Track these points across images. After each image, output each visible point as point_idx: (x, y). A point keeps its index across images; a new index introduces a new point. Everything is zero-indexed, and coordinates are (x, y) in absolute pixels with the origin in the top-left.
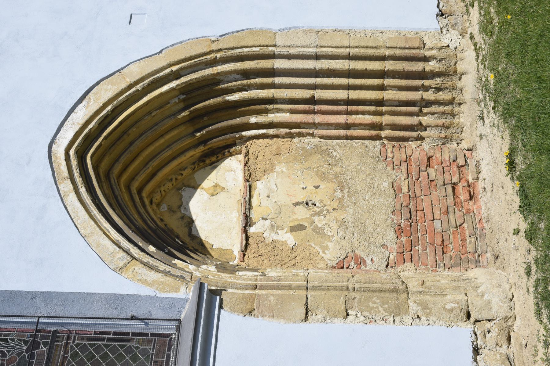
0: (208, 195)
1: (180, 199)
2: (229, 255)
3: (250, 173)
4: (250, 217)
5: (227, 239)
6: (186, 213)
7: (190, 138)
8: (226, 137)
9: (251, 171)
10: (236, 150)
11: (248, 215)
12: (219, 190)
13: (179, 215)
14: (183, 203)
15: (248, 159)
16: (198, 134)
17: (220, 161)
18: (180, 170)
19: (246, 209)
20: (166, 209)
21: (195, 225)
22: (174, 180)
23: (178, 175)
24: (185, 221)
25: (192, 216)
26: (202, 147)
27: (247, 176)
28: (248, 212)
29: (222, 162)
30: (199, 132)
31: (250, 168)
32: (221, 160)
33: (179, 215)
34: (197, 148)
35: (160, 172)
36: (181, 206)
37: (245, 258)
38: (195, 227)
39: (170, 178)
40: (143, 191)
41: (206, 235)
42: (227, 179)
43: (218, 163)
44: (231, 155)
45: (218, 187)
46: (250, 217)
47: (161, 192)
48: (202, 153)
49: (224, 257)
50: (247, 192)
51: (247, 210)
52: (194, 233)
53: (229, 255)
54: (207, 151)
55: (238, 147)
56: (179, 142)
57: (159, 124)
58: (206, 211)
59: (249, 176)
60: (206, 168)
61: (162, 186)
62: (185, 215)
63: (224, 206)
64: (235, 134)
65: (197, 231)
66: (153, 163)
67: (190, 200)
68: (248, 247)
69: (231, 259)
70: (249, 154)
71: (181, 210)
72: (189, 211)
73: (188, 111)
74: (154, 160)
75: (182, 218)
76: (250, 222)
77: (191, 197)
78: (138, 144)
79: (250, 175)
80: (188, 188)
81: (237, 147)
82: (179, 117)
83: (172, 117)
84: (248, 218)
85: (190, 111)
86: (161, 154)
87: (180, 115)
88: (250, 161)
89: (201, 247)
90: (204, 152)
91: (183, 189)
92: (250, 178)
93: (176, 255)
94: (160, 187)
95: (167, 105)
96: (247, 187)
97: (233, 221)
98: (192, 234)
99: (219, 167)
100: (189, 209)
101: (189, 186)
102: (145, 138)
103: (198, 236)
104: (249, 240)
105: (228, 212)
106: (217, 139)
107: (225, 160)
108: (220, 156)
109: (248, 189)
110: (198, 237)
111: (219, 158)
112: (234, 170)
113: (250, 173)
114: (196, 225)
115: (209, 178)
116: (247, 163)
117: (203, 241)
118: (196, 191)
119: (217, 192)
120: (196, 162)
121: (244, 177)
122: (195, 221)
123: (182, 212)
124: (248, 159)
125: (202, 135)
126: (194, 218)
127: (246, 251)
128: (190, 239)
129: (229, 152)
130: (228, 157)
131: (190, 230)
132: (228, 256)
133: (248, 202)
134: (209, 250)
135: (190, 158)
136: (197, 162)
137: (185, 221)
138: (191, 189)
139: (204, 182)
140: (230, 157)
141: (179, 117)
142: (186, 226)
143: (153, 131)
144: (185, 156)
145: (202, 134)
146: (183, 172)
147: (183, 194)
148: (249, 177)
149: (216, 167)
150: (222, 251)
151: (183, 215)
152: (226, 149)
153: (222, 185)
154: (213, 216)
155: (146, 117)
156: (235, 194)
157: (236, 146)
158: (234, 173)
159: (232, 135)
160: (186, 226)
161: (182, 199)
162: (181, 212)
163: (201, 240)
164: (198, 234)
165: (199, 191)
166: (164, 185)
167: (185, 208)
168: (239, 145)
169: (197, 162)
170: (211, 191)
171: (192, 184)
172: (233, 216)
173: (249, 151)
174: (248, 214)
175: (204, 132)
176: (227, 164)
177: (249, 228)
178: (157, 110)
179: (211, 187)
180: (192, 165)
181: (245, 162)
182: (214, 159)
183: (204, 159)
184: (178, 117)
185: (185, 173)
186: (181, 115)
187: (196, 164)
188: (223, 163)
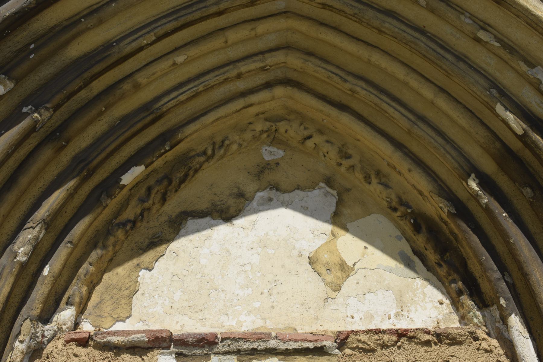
0: (313, 249)
1: (298, 186)
2: (114, 309)
3: (373, 351)
4: (212, 356)
5: (167, 302)
6: (254, 203)
7: (457, 165)
8: (492, 269)
9: (379, 352)
10: (469, 312)
11: (216, 350)
12: (329, 278)
13: (249, 187)
14: (286, 195)
15: (428, 343)
16: (474, 185)
17: (430, 275)
18: (378, 173)
19: (236, 340)
20: (267, 158)
21: (216, 225)
22: (346, 163)
23: (362, 168)
24: (231, 202)
25: (244, 216)
26: (446, 210)
27: (359, 341)
28: (226, 348)
29: (428, 280)
30: (479, 184)
31: (395, 348)
32: (434, 279)
33: (249, 187)
34: (440, 195)
35: (351, 117)
36: (278, 190)
37: (73, 346)
38: (211, 226)
39: (350, 152)
40: (289, 88)
41: (183, 251)
42: (369, 296)
43: (425, 269)
44: (456, 304)
45: (339, 274)
46: (212, 356)
47: (310, 137)
48: (437, 219)
49: (108, 298)
50: (300, 343)
51: (234, 346)
52: (191, 223)
53: (114, 309)
54: (447, 232)
55: (477, 316)
56: (440, 140)
57: (461, 63)
58: (260, 250)
59: (360, 345)
60: (404, 240)
61: (325, 138)
62: (250, 200)
63: (275, 291)
64: (509, 295)
65: (198, 231)
66: (362, 88)
67: (295, 209)
68: (109, 354)
69: (100, 316)
70: (450, 345)
71: (263, 190)
72: (261, 208)
73: (525, 126)
74: (371, 89)
75: (241, 195)
76: (194, 355)
77: (305, 210)
78: (387, 25)
79: (365, 351)
80: (334, 201)
81: (478, 313)
82: (499, 109)
83: (494, 91)
84: (203, 347)
85: (525, 134)
86: (393, 104)
87: (506, 109)
88: (422, 349)
89: (147, 241)
90: (443, 225)
91: (329, 190)
92: (353, 349)
93: (6, 131)
94: (321, 132)
95: (522, 64)
96: (316, 341)
97: (224, 318)
98: (186, 220)
99: (412, 274)
100: (267, 210)
101: (340, 203)
102: (409, 38)
103: (180, 233)
104: (133, 354)
105: (257, 305)
106: (480, 245)
107: (438, 289)
108: (443, 271)
109: (311, 345)
110: (177, 234)
111: (438, 269)
112: (405, 313)
113: (373, 351)
114: (216, 228)
115: (371, 249)
116: (410, 339)
117: (164, 246)
118: (326, 221)
119: (323, 271)
120: (410, 207)
121: (357, 332)
122: (229, 224)
123: (260, 194)
124: (428, 343)
125: (475, 197)
126: (239, 222)
127: (95, 347)
128: (174, 215)
129: (460, 293)
130: (448, 293)
131: (201, 215)
132: (108, 309)
133: (262, 346)
134: (135, 261)
135: (415, 191)
136: (409, 211)
137: (231, 202)
138: (333, 209)
139: (356, 239)
140: (447, 301)
141: (499, 109)
142: (214, 205)
143: (435, 51)
144: (410, 170)
145: (477, 195)
146: (374, 181)
147: (316, 192)
148: (357, 347)
149: (409, 265)
150: (127, 292)
151: (248, 195)
152: (464, 283)
153: (348, 286)
154: (243, 265)
155: (468, 21)
156: (316, 319)
157: (480, 309)
158: (393, 313)
159: (503, 285)
160: (214, 205)
161: (297, 191)
162: (258, 190)
163: (169, 241)
164: (187, 234)
165: (328, 228)
166: (327, 141)
167: (270, 200)
168: (484, 316)
169: (409, 211)
170: (325, 257)
171: (346, 211)
172: (243, 318)
173: (460, 343)
174: (220, 348)
175: (485, 199)
176: (424, 294)
177: (170, 354)
178: (498, 40)
179: (339, 255)
180: (396, 200)
181: (411, 334)
182: (432, 257)
183: (424, 229)
184: (499, 104)
185: (375, 187)
186: (508, 113)
187: (402, 209)
188: (425, 283)
